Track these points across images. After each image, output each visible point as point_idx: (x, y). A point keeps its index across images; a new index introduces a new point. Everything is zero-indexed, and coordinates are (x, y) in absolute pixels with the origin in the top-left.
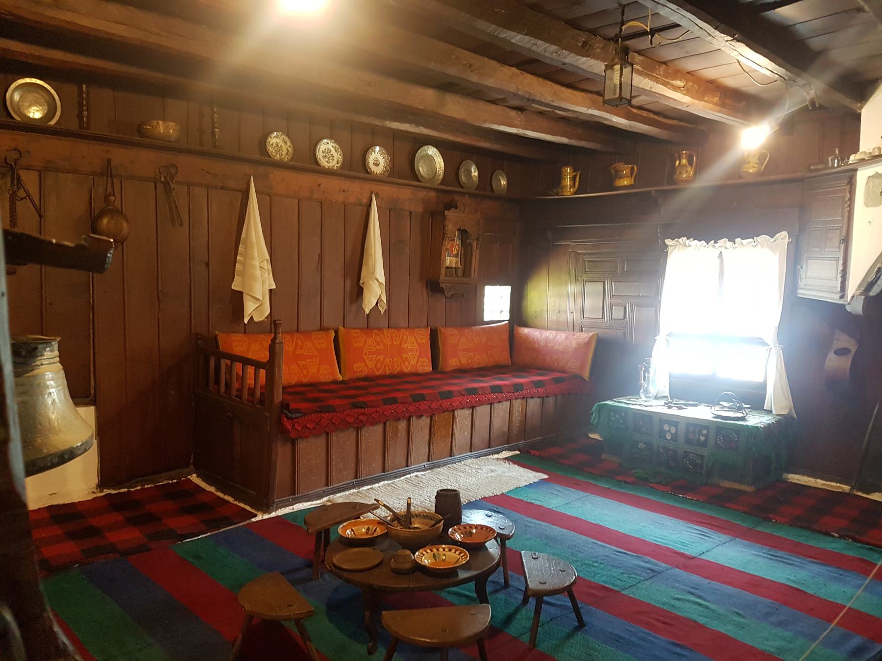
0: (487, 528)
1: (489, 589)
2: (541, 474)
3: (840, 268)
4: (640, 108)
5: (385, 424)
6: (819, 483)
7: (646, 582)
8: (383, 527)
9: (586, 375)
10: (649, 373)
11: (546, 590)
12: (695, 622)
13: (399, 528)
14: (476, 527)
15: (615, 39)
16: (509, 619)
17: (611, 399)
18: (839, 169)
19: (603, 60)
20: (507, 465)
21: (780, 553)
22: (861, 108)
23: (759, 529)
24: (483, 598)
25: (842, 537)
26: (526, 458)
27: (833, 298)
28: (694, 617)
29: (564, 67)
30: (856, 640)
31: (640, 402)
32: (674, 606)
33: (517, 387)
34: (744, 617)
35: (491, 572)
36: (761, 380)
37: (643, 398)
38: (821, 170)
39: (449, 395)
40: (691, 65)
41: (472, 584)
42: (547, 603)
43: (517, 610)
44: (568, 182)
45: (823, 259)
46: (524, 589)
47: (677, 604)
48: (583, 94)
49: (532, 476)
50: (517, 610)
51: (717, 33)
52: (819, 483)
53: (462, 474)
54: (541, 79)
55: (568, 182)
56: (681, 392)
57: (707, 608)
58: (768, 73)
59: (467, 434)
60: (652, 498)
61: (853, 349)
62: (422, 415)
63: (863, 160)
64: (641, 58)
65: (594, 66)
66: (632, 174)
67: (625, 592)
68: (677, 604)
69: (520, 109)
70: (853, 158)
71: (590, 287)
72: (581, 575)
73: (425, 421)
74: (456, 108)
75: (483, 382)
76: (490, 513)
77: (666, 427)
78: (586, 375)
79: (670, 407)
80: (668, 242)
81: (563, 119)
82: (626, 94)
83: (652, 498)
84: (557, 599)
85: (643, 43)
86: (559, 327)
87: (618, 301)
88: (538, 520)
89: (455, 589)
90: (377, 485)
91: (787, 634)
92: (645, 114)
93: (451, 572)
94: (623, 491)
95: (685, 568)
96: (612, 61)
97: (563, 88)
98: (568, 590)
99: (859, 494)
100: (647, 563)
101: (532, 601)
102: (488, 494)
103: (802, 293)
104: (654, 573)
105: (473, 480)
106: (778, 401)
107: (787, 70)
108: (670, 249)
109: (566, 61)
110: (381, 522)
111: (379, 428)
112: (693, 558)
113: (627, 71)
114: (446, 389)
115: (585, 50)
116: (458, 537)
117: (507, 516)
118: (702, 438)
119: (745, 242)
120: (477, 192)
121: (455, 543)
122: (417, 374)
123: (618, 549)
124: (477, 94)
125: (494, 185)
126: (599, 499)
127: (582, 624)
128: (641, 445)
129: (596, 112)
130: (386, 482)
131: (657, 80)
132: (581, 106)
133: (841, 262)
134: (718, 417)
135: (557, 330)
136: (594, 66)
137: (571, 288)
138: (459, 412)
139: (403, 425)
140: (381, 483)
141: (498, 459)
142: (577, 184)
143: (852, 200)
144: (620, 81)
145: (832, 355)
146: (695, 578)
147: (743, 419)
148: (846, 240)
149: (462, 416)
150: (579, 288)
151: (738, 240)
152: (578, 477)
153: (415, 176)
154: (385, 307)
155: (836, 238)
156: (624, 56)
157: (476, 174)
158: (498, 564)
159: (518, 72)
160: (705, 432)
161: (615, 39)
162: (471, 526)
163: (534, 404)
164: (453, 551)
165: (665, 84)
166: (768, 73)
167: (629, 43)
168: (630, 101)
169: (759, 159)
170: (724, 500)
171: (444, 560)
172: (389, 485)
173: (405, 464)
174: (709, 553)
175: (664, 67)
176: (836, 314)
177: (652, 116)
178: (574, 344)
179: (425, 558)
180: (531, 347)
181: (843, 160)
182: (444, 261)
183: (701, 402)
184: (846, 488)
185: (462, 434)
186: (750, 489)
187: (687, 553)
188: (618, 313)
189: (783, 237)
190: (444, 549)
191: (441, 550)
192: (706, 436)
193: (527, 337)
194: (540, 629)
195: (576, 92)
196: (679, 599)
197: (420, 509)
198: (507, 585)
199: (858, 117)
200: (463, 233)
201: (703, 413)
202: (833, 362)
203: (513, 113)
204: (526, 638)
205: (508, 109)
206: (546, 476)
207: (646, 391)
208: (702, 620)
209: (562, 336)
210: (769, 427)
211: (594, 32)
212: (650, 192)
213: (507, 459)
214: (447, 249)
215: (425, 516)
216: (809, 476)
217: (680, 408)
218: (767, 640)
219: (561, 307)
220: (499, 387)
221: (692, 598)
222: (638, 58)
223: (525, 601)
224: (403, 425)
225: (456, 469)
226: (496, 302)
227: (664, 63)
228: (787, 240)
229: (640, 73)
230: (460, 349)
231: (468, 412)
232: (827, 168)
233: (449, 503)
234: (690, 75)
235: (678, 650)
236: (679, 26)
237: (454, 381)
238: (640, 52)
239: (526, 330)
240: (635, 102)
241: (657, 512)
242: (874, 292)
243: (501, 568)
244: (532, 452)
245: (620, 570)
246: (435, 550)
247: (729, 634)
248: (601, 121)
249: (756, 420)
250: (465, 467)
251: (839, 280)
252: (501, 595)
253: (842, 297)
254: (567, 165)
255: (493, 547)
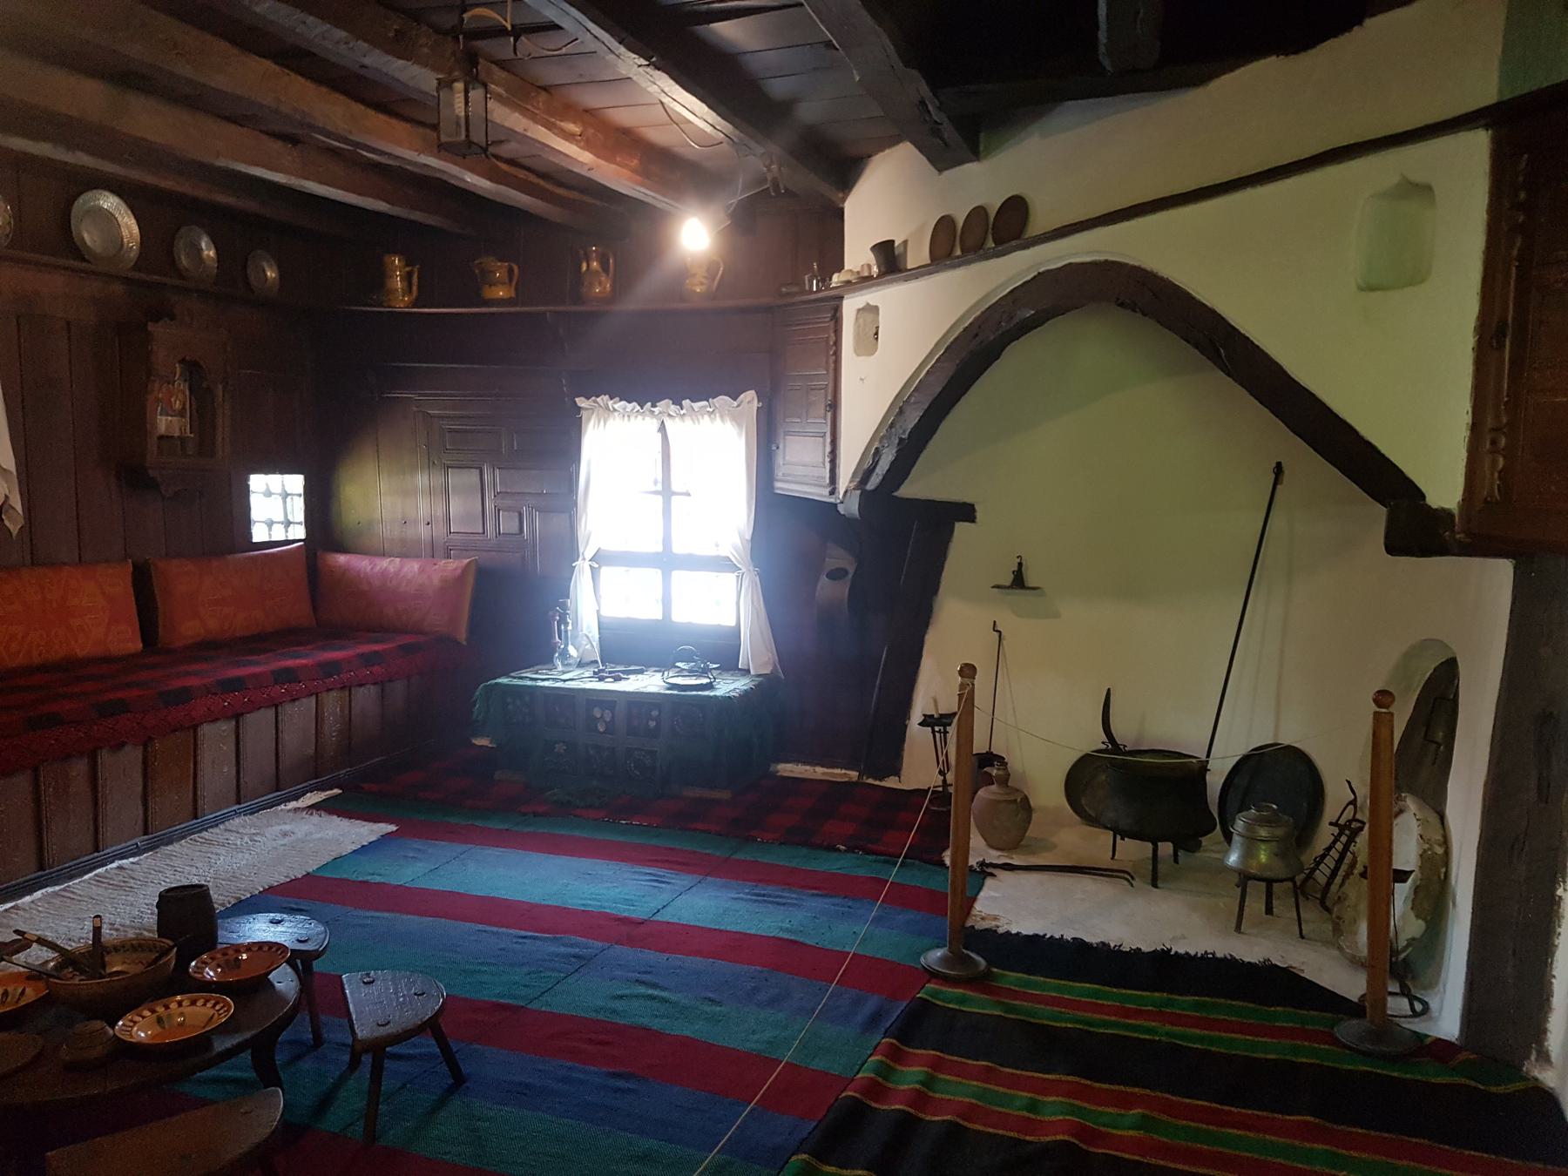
0: (271, 945)
1: (280, 1059)
2: (382, 825)
3: (828, 449)
4: (511, 162)
5: (36, 770)
6: (819, 772)
7: (569, 980)
8: (41, 985)
9: (462, 636)
10: (566, 624)
11: (389, 1036)
12: (648, 1030)
13: (76, 981)
14: (249, 948)
15: (453, 33)
16: (325, 1103)
17: (506, 675)
18: (820, 295)
19: (435, 69)
20: (315, 818)
21: (770, 890)
22: (844, 200)
23: (740, 856)
24: (268, 1076)
25: (850, 849)
26: (349, 803)
27: (820, 493)
28: (645, 1021)
29: (363, 72)
30: (872, 1003)
31: (554, 674)
32: (614, 1011)
33: (329, 668)
34: (720, 1004)
35: (283, 1021)
36: (733, 623)
37: (560, 668)
38: (795, 294)
39: (183, 697)
40: (591, 98)
41: (246, 1056)
42: (399, 1057)
43: (342, 1079)
44: (398, 283)
45: (805, 434)
46: (350, 1041)
47: (619, 1005)
48: (408, 125)
49: (359, 833)
50: (342, 1079)
51: (622, 49)
52: (819, 772)
53: (222, 851)
54: (324, 89)
55: (398, 283)
56: (622, 648)
57: (665, 1001)
58: (709, 129)
59: (229, 769)
60: (577, 833)
61: (851, 571)
62: (123, 744)
63: (849, 282)
64: (504, 75)
65: (418, 76)
66: (511, 280)
67: (534, 1006)
68: (619, 1005)
69: (293, 140)
70: (836, 279)
71: (457, 478)
72: (457, 992)
73: (132, 756)
74: (150, 121)
75: (258, 663)
76: (278, 916)
77: (597, 713)
78: (462, 636)
79: (601, 679)
80: (581, 402)
81: (377, 166)
82: (478, 137)
83: (577, 833)
84: (415, 1046)
85: (502, 48)
86: (406, 550)
87: (508, 502)
88: (377, 910)
89: (213, 1072)
90: (28, 899)
91: (781, 1016)
92: (522, 174)
93: (201, 1043)
94: (531, 829)
95: (631, 941)
96: (450, 73)
97: (371, 112)
98: (432, 1026)
99: (870, 781)
100: (572, 946)
101: (367, 1059)
102: (278, 878)
103: (781, 487)
104: (582, 962)
105: (243, 859)
106: (756, 653)
107: (736, 126)
108: (584, 414)
109: (367, 61)
110: (35, 975)
111: (22, 781)
112: (642, 923)
113: (476, 94)
114: (176, 684)
115: (400, 46)
116: (210, 974)
117: (312, 915)
118: (652, 724)
119: (697, 405)
120: (130, 274)
121: (207, 986)
122: (107, 660)
123: (523, 933)
124: (195, 100)
125: (252, 278)
126: (492, 852)
127: (459, 1080)
128: (560, 748)
129: (433, 162)
130: (50, 890)
131: (534, 118)
132: (405, 148)
133: (828, 440)
134: (673, 686)
135: (403, 555)
136: (418, 76)
137: (421, 480)
138: (207, 730)
139: (79, 768)
140: (38, 894)
141: (296, 810)
142: (415, 288)
143: (838, 343)
144: (466, 112)
145: (824, 579)
146: (651, 956)
147: (710, 686)
148: (834, 406)
149: (215, 737)
150: (438, 479)
151: (686, 402)
152: (453, 820)
153: (76, 250)
154: (21, 522)
155: (820, 401)
156: (470, 68)
157: (212, 253)
158: (296, 1009)
159: (277, 68)
160: (655, 713)
161: (453, 33)
162: (238, 949)
163: (365, 697)
164: (200, 1003)
165: (550, 127)
166: (709, 129)
167: (479, 44)
168: (485, 150)
169: (708, 271)
170: (687, 818)
171: (181, 1024)
172: (56, 894)
173: (90, 846)
174: (669, 909)
175: (543, 96)
176: (820, 514)
177: (532, 178)
178: (436, 581)
179: (139, 1029)
180: (352, 588)
181: (823, 280)
182: (154, 425)
183: (648, 666)
184: (854, 774)
185: (216, 767)
186: (725, 795)
187: (634, 916)
188: (508, 524)
189: (750, 399)
190: (180, 1004)
191: (173, 1006)
192: (658, 719)
193: (345, 571)
194: (383, 1108)
195: (394, 121)
196: (621, 997)
197: (131, 934)
198: (318, 1040)
199: (840, 214)
200: (193, 369)
201: (650, 683)
202: (827, 590)
203: (277, 145)
204: (359, 1128)
205: (265, 137)
206: (393, 828)
207: (564, 654)
208: (656, 1024)
209: (412, 567)
210: (746, 694)
211: (416, 16)
212: (544, 313)
213: (315, 807)
214: (158, 400)
215: (135, 946)
216: (805, 763)
217: (618, 679)
218: (754, 1032)
219: (411, 511)
220: (287, 670)
221: (642, 990)
222: (499, 74)
223: (354, 1063)
224: (79, 768)
225: (209, 842)
226: (275, 506)
227: (545, 89)
228: (755, 404)
229: (499, 98)
230: (201, 602)
231: (226, 727)
232: (803, 292)
233: (189, 915)
234: (589, 116)
235: (621, 1083)
236: (559, 28)
237: (195, 667)
238: (502, 64)
239: (342, 559)
240: (491, 149)
241: (580, 856)
242: (871, 486)
243: (304, 1018)
244: (366, 786)
245: (525, 969)
246: (160, 1009)
247: (698, 1036)
248: (445, 177)
249: (728, 687)
250: (227, 835)
251: (828, 466)
252: (306, 1065)
253: (832, 493)
254: (395, 253)
255: (284, 980)
